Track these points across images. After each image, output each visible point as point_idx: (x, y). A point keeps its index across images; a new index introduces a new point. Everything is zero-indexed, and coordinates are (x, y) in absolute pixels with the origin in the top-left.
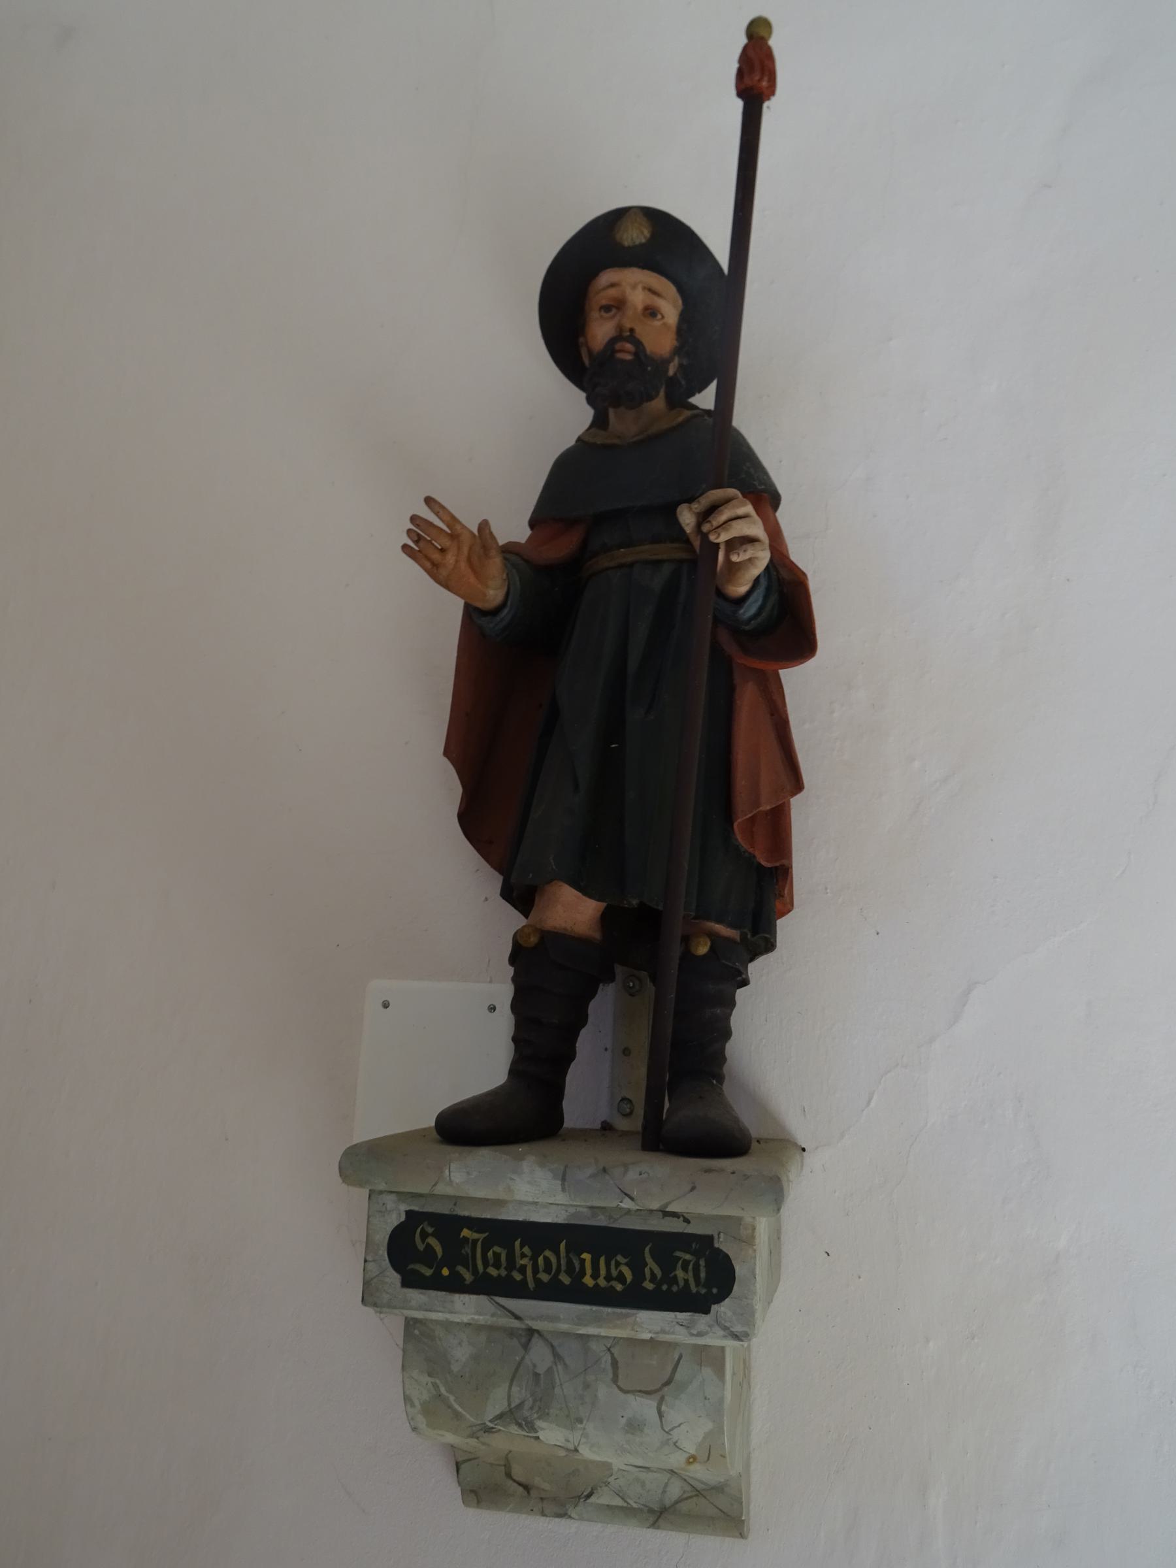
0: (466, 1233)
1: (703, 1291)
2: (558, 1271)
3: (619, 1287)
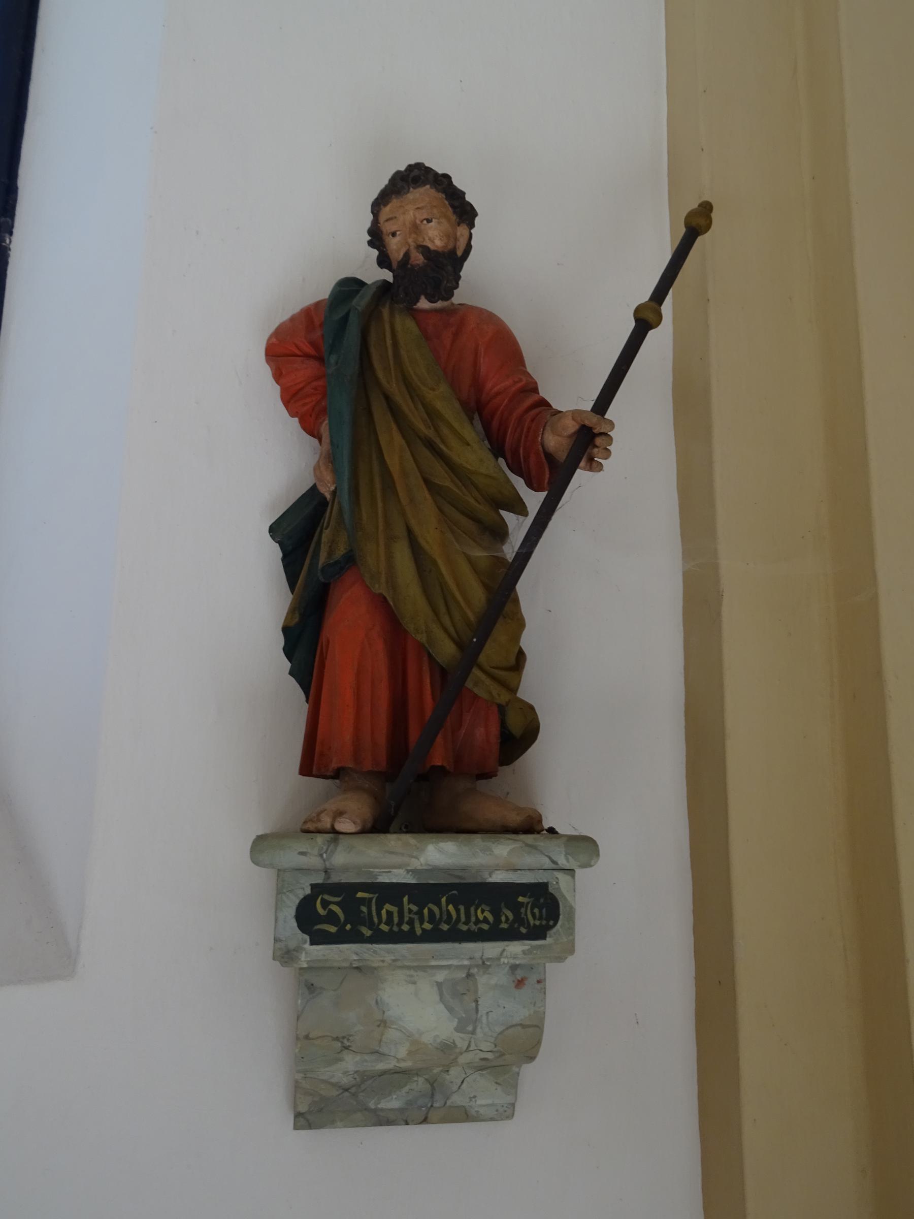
0: (360, 895)
3: (485, 927)
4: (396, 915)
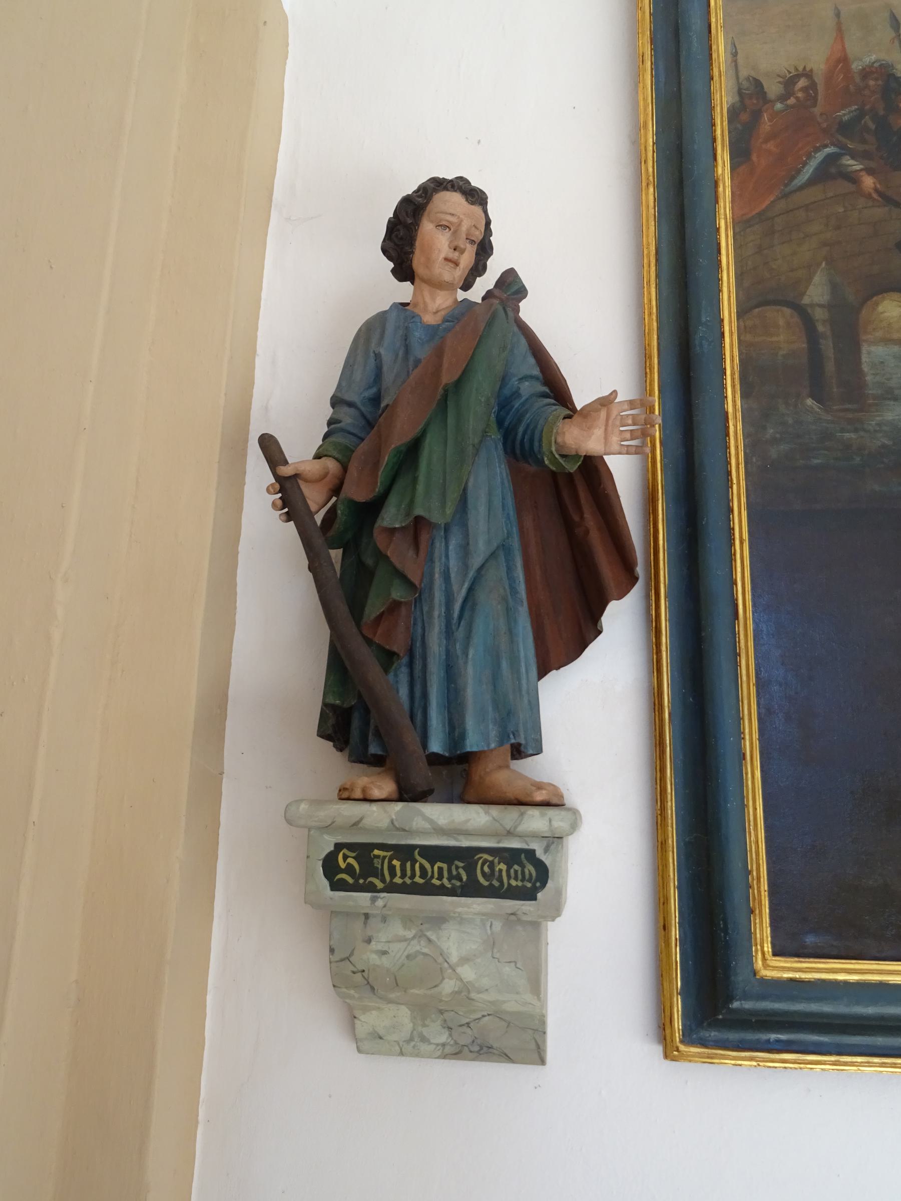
0: (376, 852)
1: (529, 885)
2: (432, 877)
4: (519, 872)
